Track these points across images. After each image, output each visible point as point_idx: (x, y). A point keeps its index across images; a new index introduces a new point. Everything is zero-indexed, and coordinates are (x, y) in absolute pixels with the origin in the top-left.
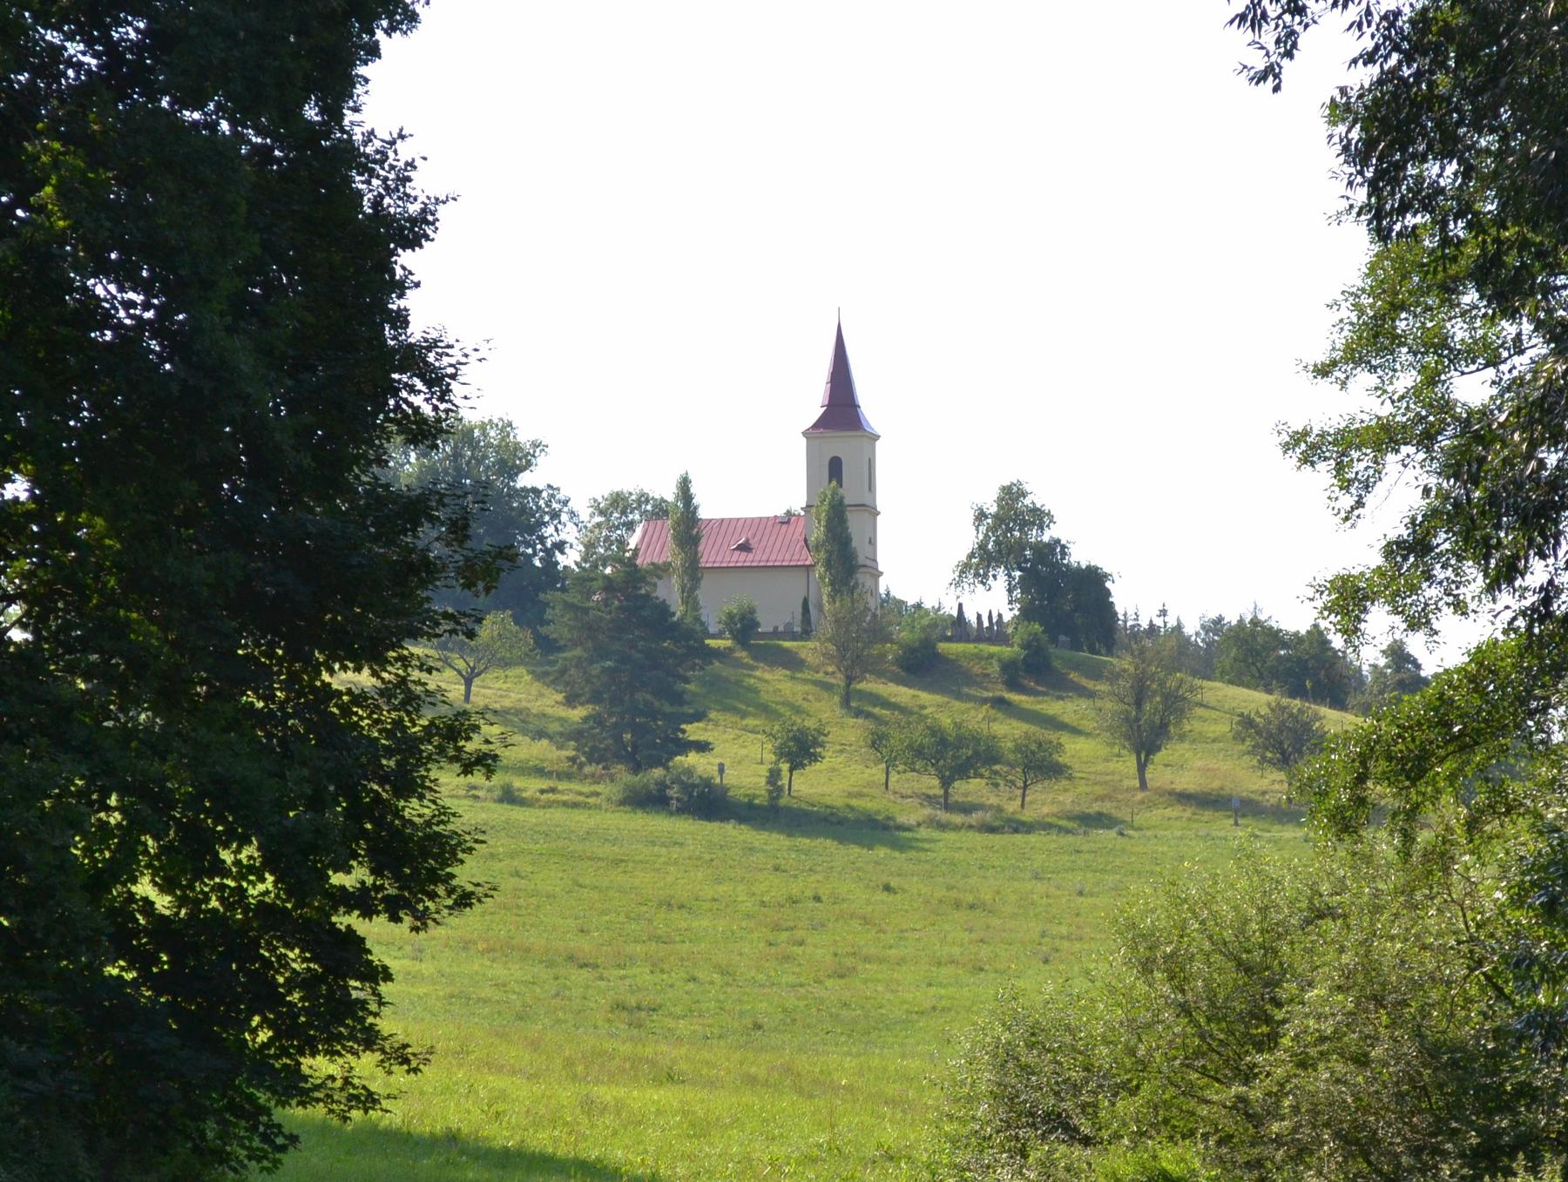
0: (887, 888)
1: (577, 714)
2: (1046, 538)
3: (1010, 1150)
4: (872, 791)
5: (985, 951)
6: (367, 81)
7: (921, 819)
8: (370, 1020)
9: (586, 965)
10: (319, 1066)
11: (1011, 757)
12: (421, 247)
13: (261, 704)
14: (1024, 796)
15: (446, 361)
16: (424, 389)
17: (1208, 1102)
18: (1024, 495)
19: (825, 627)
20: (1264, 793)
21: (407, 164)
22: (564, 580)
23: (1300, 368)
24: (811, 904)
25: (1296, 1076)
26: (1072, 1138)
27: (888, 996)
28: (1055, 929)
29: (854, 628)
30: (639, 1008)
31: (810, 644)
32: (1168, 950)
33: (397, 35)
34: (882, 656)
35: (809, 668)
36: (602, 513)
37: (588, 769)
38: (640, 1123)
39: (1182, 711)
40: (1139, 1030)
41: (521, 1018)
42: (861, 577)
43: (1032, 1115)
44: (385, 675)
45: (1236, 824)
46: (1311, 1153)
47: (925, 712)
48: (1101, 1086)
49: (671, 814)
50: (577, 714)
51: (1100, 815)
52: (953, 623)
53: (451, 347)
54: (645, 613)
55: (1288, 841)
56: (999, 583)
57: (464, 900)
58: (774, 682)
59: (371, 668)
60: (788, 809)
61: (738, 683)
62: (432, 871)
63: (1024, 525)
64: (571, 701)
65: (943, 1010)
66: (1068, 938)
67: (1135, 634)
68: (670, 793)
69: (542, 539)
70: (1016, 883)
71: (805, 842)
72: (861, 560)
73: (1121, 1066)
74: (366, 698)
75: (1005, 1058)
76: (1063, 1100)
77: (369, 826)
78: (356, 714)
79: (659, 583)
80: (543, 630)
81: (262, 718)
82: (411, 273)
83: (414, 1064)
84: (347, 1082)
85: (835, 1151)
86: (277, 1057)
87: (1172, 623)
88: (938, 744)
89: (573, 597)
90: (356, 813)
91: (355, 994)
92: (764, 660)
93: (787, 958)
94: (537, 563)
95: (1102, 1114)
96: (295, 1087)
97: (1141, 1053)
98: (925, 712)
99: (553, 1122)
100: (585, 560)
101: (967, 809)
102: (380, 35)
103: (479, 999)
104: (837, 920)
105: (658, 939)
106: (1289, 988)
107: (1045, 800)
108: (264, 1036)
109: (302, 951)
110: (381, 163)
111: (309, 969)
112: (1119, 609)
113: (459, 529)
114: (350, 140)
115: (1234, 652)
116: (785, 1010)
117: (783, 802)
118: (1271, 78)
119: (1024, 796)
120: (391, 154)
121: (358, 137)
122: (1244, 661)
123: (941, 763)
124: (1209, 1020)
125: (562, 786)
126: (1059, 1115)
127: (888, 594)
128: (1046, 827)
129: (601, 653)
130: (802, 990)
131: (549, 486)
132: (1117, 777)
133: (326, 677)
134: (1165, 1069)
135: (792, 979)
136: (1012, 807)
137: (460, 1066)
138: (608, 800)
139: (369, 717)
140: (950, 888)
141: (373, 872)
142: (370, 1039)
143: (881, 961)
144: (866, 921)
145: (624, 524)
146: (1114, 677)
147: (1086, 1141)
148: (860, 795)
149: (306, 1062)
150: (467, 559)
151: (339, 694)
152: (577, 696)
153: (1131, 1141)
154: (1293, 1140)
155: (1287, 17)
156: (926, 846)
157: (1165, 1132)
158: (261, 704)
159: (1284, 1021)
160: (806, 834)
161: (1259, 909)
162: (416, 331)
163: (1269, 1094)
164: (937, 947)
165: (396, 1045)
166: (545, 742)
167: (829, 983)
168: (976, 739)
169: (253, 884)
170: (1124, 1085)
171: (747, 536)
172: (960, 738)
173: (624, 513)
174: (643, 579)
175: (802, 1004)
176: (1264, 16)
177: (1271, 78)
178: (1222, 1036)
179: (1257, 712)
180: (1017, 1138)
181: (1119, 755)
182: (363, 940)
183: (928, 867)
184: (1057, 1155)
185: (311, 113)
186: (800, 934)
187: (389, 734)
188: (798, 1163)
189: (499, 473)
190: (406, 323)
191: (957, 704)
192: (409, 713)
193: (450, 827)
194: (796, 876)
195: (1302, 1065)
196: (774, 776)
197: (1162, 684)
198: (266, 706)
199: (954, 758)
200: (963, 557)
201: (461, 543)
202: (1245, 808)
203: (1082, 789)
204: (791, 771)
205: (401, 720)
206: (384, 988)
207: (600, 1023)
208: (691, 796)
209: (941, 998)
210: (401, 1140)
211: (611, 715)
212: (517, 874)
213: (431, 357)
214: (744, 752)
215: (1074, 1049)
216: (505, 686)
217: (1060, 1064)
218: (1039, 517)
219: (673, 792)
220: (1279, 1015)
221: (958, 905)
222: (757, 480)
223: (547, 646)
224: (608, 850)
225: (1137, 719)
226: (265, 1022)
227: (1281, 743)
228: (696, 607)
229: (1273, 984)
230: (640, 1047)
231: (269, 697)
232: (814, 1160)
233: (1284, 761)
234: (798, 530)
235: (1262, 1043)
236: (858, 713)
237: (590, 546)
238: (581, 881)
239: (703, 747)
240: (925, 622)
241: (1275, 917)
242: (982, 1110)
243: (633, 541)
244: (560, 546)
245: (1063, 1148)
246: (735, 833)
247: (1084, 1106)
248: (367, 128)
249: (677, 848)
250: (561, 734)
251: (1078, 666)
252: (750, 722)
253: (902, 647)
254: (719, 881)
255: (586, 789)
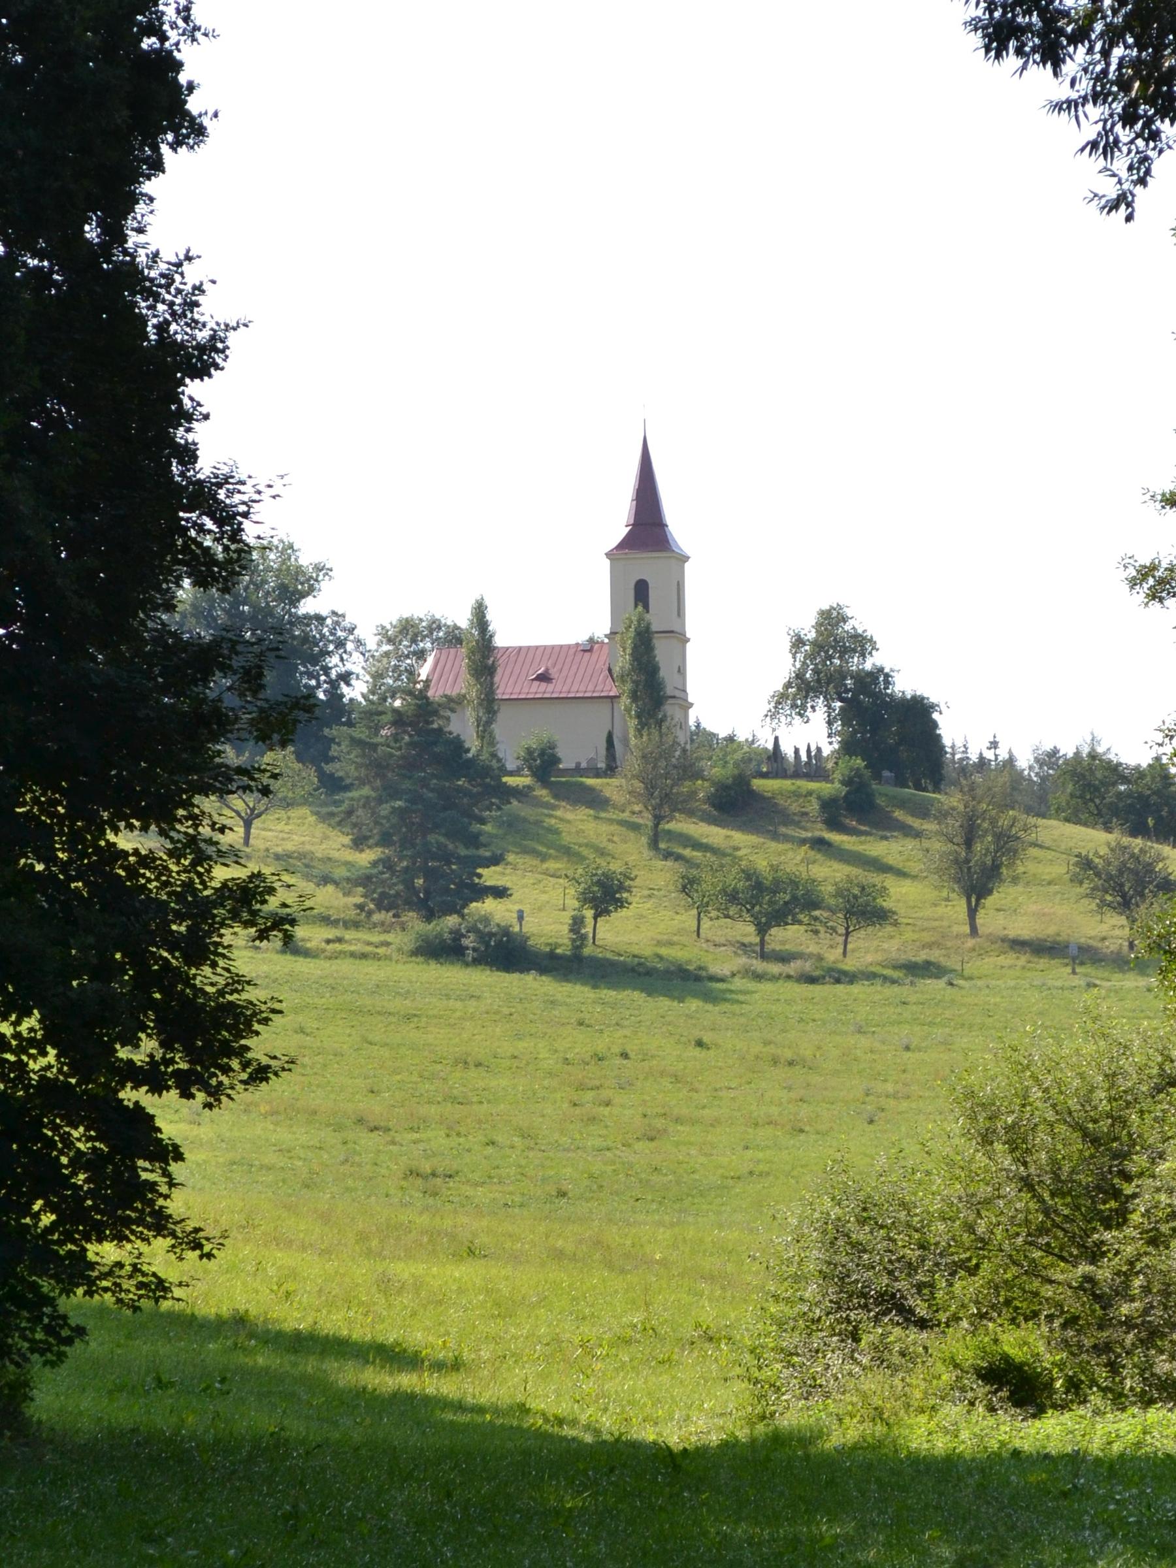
0: (700, 1044)
1: (366, 858)
2: (868, 666)
3: (840, 1334)
4: (684, 939)
5: (805, 1111)
6: (151, 199)
7: (735, 969)
8: (160, 1202)
9: (376, 1128)
10: (105, 1252)
11: (832, 902)
12: (210, 376)
13: (39, 867)
14: (846, 943)
15: (237, 498)
16: (214, 528)
17: (1051, 1282)
18: (844, 619)
19: (631, 762)
20: (1104, 939)
21: (195, 288)
22: (350, 713)
23: (1148, 497)
24: (618, 1061)
25: (1146, 1254)
26: (907, 1320)
27: (702, 1159)
28: (880, 1087)
29: (662, 763)
30: (434, 1175)
31: (615, 782)
32: (1010, 1120)
33: (183, 150)
34: (693, 794)
35: (615, 807)
36: (390, 641)
37: (376, 917)
38: (440, 1302)
39: (1016, 851)
40: (980, 1205)
41: (307, 1186)
42: (669, 709)
43: (864, 1295)
44: (173, 834)
45: (1074, 972)
46: (1163, 1336)
47: (739, 853)
48: (937, 1264)
49: (467, 965)
50: (366, 858)
51: (928, 963)
52: (769, 758)
53: (243, 483)
54: (437, 749)
55: (1129, 991)
56: (818, 715)
57: (261, 1074)
58: (575, 822)
59: (158, 826)
60: (593, 960)
61: (538, 823)
62: (226, 1042)
63: (845, 652)
64: (359, 843)
65: (761, 1175)
66: (895, 1096)
67: (965, 769)
68: (465, 942)
69: (326, 670)
70: (838, 1038)
71: (609, 994)
72: (669, 691)
73: (960, 1244)
74: (154, 859)
75: (835, 1234)
76: (896, 1279)
77: (157, 996)
78: (143, 876)
79: (453, 716)
80: (328, 768)
81: (46, 879)
82: (199, 404)
83: (206, 1249)
84: (136, 1269)
85: (650, 1331)
86: (61, 1243)
87: (1003, 755)
88: (754, 888)
89: (360, 732)
90: (144, 981)
91: (144, 1176)
92: (567, 798)
93: (593, 1120)
94: (321, 696)
95: (939, 1294)
96: (79, 1272)
97: (981, 1230)
98: (739, 853)
99: (348, 1302)
100: (373, 693)
101: (783, 958)
102: (165, 149)
103: (262, 1167)
104: (646, 1079)
105: (455, 1100)
106: (1139, 1161)
107: (869, 948)
108: (47, 1219)
109: (87, 1129)
110: (167, 287)
111: (94, 1148)
112: (947, 741)
113: (252, 679)
114: (133, 263)
115: (1070, 788)
116: (591, 1176)
117: (587, 951)
118: (1123, 207)
119: (846, 943)
120: (177, 277)
121: (142, 259)
122: (1081, 797)
123: (757, 908)
124: (1053, 1195)
125: (349, 935)
126: (893, 1296)
127: (698, 726)
128: (871, 976)
129: (392, 792)
130: (608, 1154)
131: (334, 613)
132: (945, 923)
133: (111, 837)
134: (1006, 1246)
135: (598, 1142)
136: (833, 956)
137: (247, 1241)
138: (399, 950)
139: (157, 879)
140: (767, 1043)
141: (162, 1044)
142: (161, 1223)
143: (694, 1122)
144: (677, 1079)
145: (415, 653)
146: (943, 815)
147: (923, 1324)
148: (670, 944)
149: (93, 1250)
150: (261, 710)
151: (125, 854)
152: (366, 838)
153: (972, 1324)
154: (1143, 1322)
155: (1140, 143)
156: (741, 997)
157: (1007, 1313)
158: (39, 867)
159: (1135, 1196)
160: (613, 986)
161: (1106, 1076)
162: (205, 467)
163: (1118, 1273)
164: (753, 1107)
165: (189, 1229)
166: (330, 888)
167: (639, 1146)
168: (794, 883)
169: (35, 1059)
170: (962, 1264)
171: (547, 664)
172: (777, 882)
173: (414, 641)
174: (435, 713)
175: (609, 1168)
176: (1117, 141)
177: (1123, 207)
178: (1066, 1212)
179: (1096, 853)
180: (849, 1322)
181: (947, 899)
182: (152, 1118)
183: (743, 1020)
184: (891, 1338)
185: (91, 232)
186: (605, 1094)
187: (180, 898)
188: (611, 1346)
189: (280, 599)
190: (194, 458)
191: (773, 845)
192: (200, 875)
193: (244, 996)
194: (601, 1031)
195: (1153, 1242)
196: (577, 923)
197: (993, 822)
198: (47, 868)
199: (771, 903)
200: (779, 687)
201: (255, 693)
202: (1084, 955)
203: (909, 935)
204: (595, 918)
205: (191, 881)
206: (174, 1167)
207: (392, 1191)
208: (487, 945)
209: (759, 1161)
210: (189, 1324)
211: (401, 859)
212: (302, 1031)
213: (222, 494)
214: (544, 897)
215: (909, 1225)
216: (287, 828)
217: (894, 1241)
218: (861, 644)
219: (469, 941)
220: (1128, 1189)
221: (775, 1061)
222: (559, 606)
223: (332, 785)
224: (397, 1005)
225: (967, 861)
226: (49, 1207)
227: (1122, 885)
228: (492, 743)
229: (1124, 1156)
230: (438, 1219)
231: (49, 858)
232: (628, 1342)
233: (1125, 905)
234: (600, 660)
235: (1109, 1218)
236: (667, 855)
237: (377, 676)
238: (370, 1037)
239: (500, 893)
240: (738, 756)
241: (1123, 1084)
242: (811, 1291)
243: (424, 672)
244: (346, 677)
245: (897, 1331)
246: (535, 985)
247: (920, 1287)
248: (152, 248)
249: (473, 1003)
250: (348, 880)
251: (903, 804)
252: (552, 865)
253: (714, 784)
254: (519, 1037)
255: (376, 938)
